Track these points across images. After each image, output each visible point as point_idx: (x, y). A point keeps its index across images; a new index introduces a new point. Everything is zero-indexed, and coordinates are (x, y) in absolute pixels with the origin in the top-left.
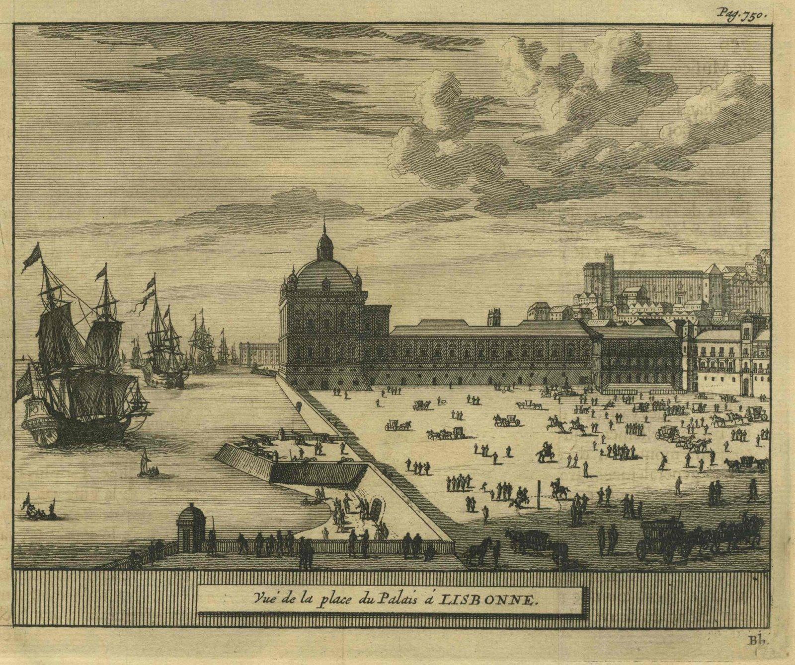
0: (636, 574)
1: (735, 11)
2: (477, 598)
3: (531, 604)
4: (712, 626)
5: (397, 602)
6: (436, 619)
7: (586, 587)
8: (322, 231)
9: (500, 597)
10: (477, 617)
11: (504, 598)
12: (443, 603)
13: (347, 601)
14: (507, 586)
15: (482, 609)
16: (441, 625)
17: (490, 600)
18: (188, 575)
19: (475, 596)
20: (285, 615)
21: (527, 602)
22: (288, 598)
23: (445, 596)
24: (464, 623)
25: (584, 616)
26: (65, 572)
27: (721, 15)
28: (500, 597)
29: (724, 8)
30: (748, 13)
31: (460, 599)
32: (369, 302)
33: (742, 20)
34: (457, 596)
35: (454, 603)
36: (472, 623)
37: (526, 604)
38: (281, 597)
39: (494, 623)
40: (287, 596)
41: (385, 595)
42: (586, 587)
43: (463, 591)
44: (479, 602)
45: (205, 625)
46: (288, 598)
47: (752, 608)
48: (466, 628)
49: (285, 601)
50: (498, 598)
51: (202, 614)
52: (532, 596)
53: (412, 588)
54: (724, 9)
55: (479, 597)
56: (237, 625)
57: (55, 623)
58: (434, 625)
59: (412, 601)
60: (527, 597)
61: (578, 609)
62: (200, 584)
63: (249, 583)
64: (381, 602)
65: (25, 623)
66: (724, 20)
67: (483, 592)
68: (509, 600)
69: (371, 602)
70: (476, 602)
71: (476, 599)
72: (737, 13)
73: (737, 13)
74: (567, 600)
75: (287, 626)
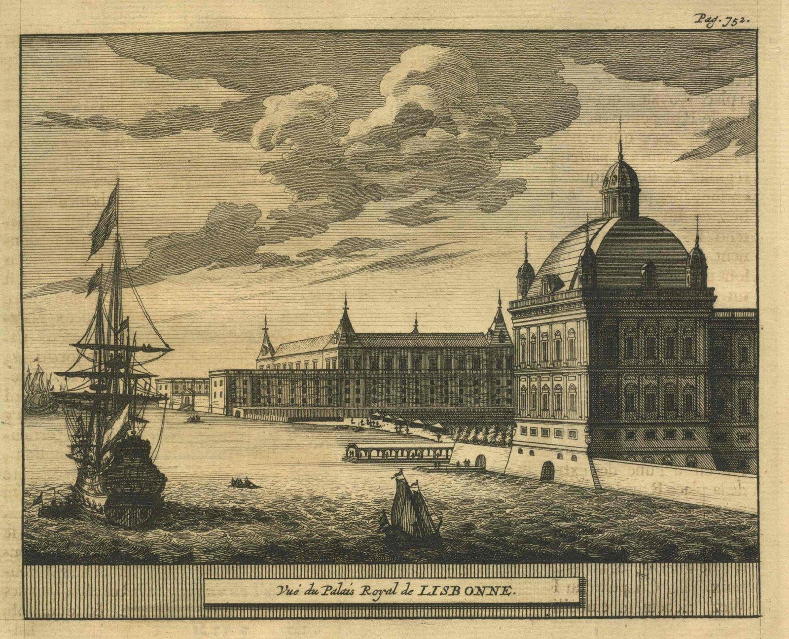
0: (367, 566)
2: (457, 588)
3: (509, 594)
4: (558, 615)
5: (338, 594)
8: (523, 257)
9: (479, 588)
10: (453, 606)
11: (482, 589)
12: (422, 594)
13: (346, 593)
14: (388, 578)
15: (461, 598)
16: (415, 615)
18: (528, 568)
19: (455, 587)
20: (453, 606)
22: (406, 590)
23: (424, 587)
24: (440, 613)
25: (580, 605)
27: (699, 21)
28: (479, 588)
30: (731, 18)
31: (438, 591)
32: (717, 305)
33: (723, 26)
34: (436, 588)
35: (433, 594)
36: (282, 613)
37: (503, 594)
38: (303, 590)
39: (236, 613)
40: (406, 588)
41: (366, 589)
43: (443, 583)
44: (459, 593)
46: (406, 590)
47: (41, 600)
48: (325, 618)
49: (405, 593)
50: (477, 589)
52: (510, 587)
53: (349, 581)
54: (703, 15)
55: (459, 588)
58: (360, 616)
59: (350, 592)
60: (505, 587)
62: (208, 578)
64: (325, 594)
65: (173, 617)
67: (463, 584)
68: (488, 591)
69: (315, 593)
70: (456, 593)
71: (457, 590)
72: (716, 19)
73: (716, 19)
74: (565, 589)
75: (109, 617)
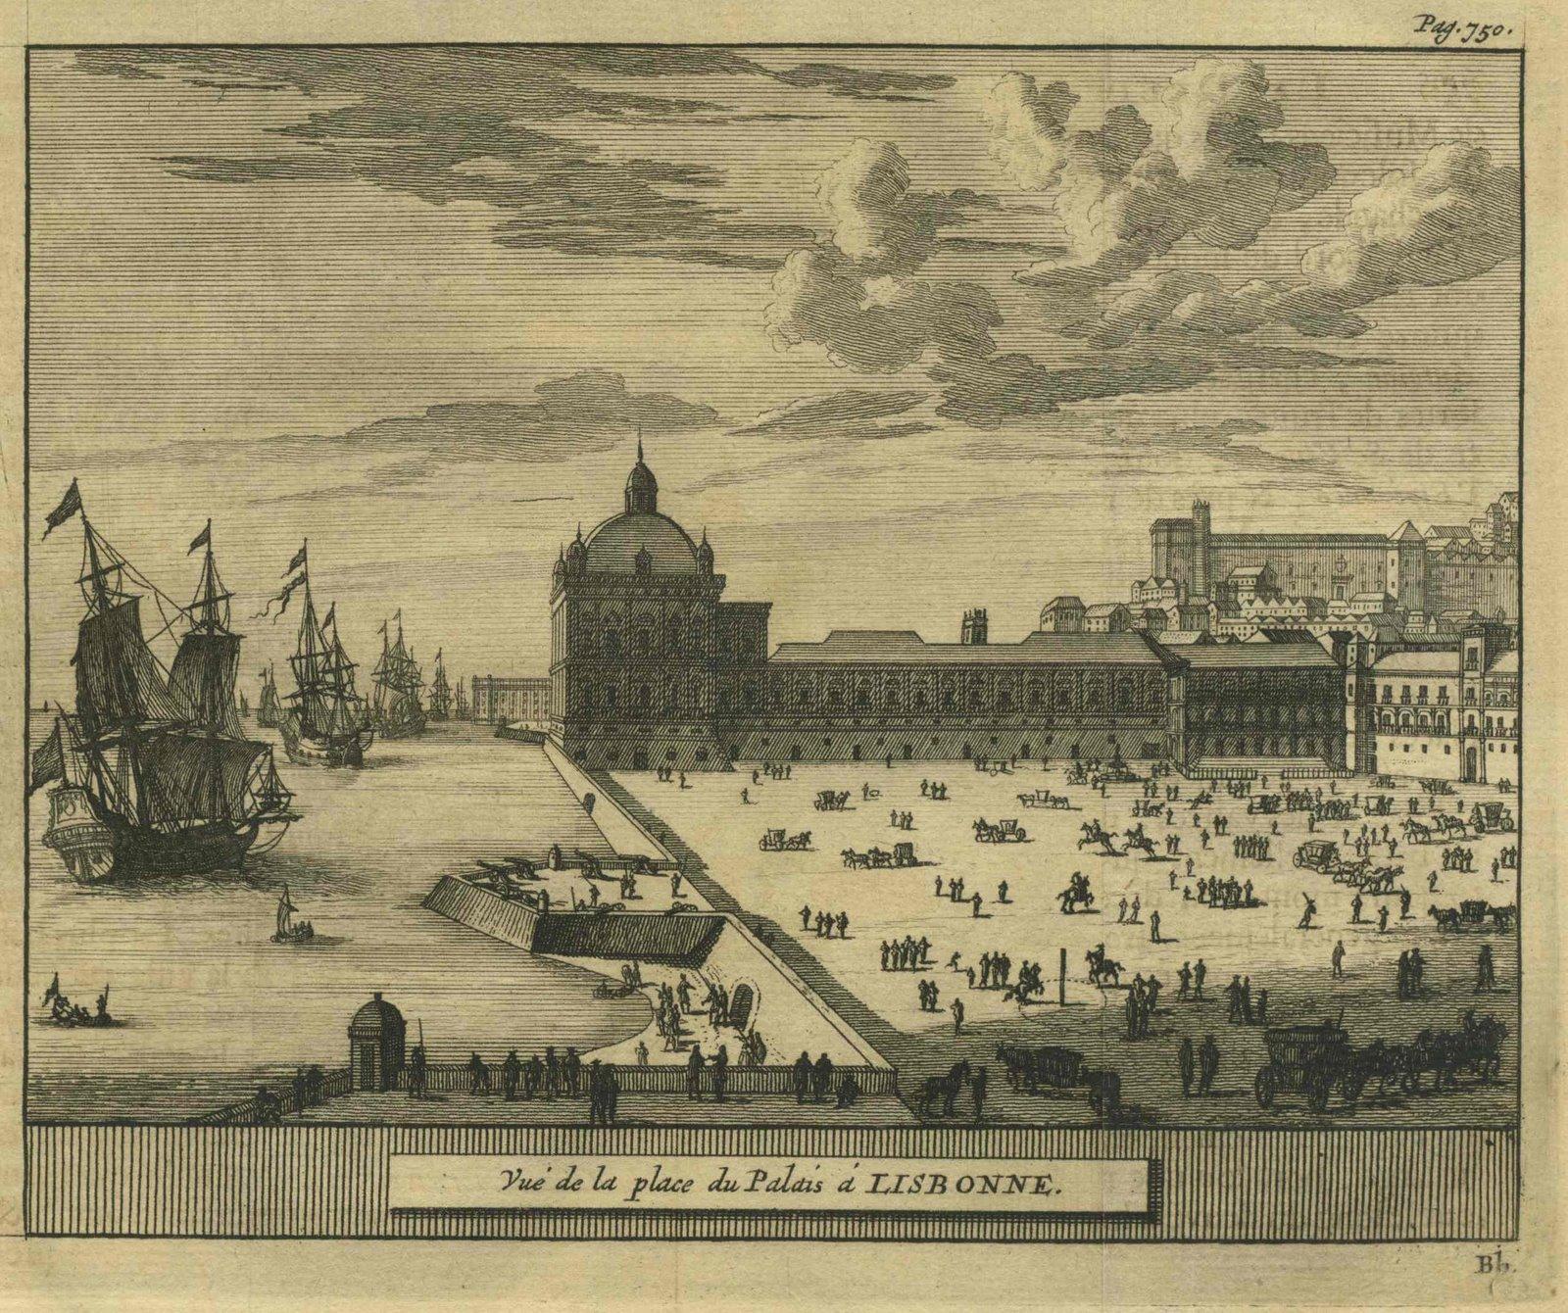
0: (1254, 1134)
1: (1450, 21)
2: (940, 1181)
3: (1047, 1193)
4: (1404, 1235)
5: (784, 1189)
6: (860, 1221)
7: (1157, 1160)
9: (986, 1178)
10: (940, 1218)
11: (993, 1181)
12: (874, 1191)
13: (685, 1186)
14: (1000, 1157)
15: (951, 1201)
16: (869, 1234)
17: (966, 1185)
18: (370, 1136)
19: (936, 1177)
20: (563, 1214)
21: (1040, 1188)
22: (568, 1180)
23: (878, 1176)
24: (915, 1229)
25: (1151, 1215)
26: (128, 1130)
27: (1421, 29)
28: (986, 1178)
29: (1428, 17)
30: (1476, 26)
31: (907, 1183)
32: (727, 596)
33: (1464, 40)
34: (901, 1177)
35: (896, 1191)
36: (930, 1230)
37: (1037, 1192)
38: (554, 1178)
39: (975, 1229)
40: (566, 1176)
41: (760, 1175)
42: (1157, 1160)
43: (913, 1167)
44: (944, 1189)
45: (404, 1233)
46: (568, 1180)
47: (1484, 1200)
48: (919, 1240)
49: (563, 1186)
50: (983, 1181)
51: (399, 1212)
52: (1049, 1177)
53: (812, 1162)
54: (1428, 19)
55: (945, 1179)
56: (468, 1234)
57: (108, 1230)
58: (856, 1235)
59: (813, 1186)
60: (1039, 1178)
61: (1139, 1203)
62: (395, 1154)
63: (490, 1151)
64: (752, 1189)
65: (50, 1231)
66: (1427, 39)
67: (953, 1169)
68: (1004, 1185)
69: (732, 1188)
70: (938, 1189)
71: (939, 1183)
72: (1453, 25)
73: (1453, 25)
74: (1119, 1184)
75: (565, 1235)
